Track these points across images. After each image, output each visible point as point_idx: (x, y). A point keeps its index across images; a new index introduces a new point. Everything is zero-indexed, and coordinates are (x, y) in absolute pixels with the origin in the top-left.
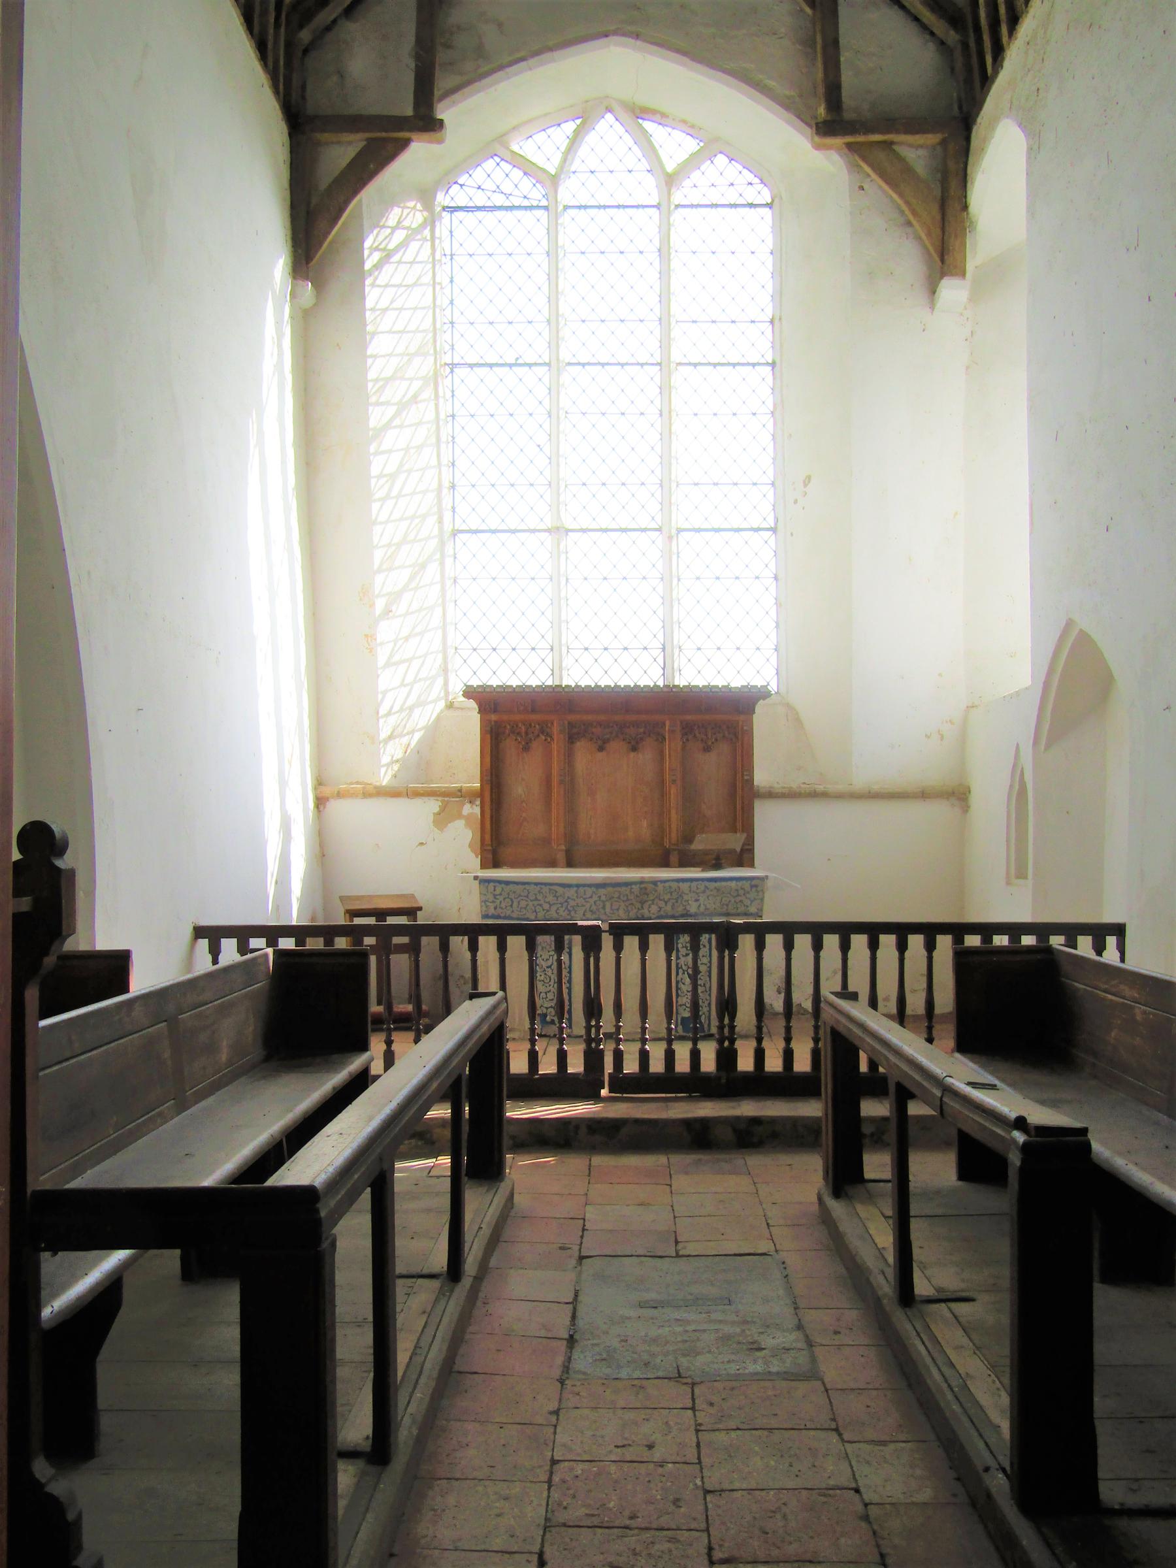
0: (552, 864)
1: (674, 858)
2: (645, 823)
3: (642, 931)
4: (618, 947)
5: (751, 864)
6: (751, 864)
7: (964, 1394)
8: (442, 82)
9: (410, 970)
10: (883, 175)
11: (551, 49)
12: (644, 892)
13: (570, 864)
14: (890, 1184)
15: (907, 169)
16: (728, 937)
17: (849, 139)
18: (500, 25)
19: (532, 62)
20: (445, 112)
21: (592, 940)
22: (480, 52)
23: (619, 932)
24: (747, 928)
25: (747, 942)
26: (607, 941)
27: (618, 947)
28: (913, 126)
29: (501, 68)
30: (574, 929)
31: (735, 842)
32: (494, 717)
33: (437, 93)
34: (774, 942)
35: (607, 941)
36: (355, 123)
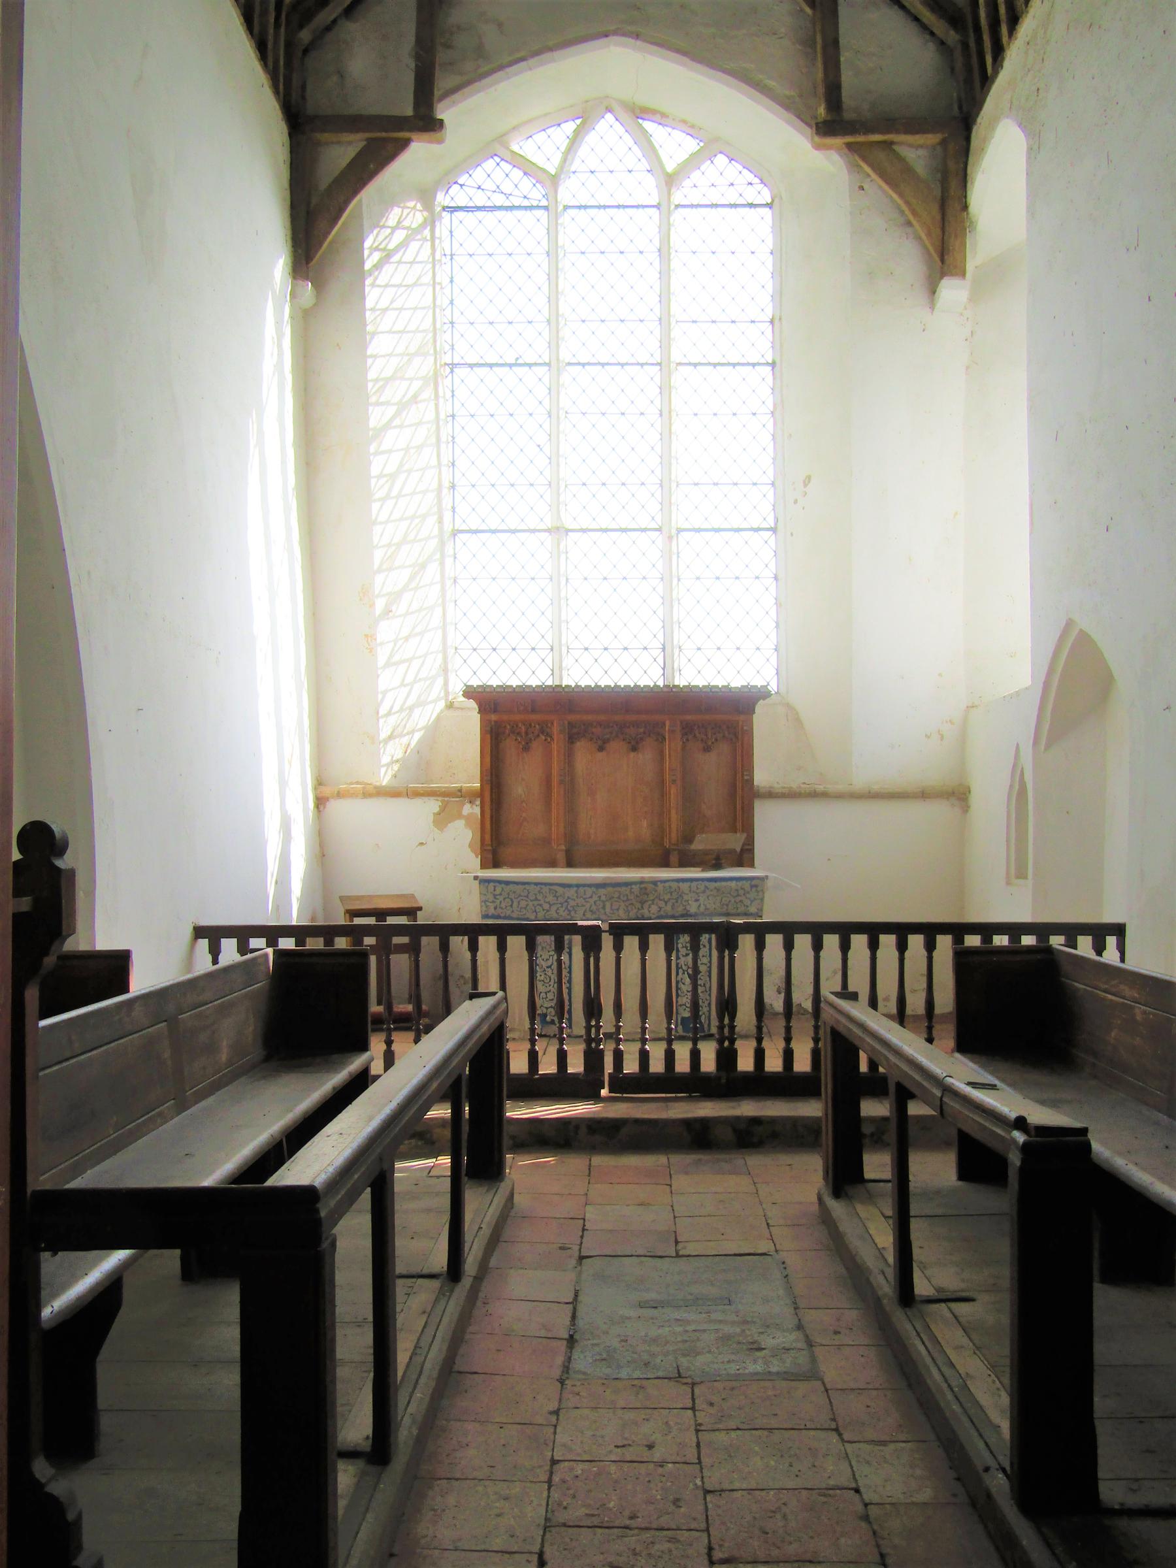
0: (552, 864)
1: (674, 858)
2: (645, 823)
3: (642, 931)
4: (618, 947)
5: (751, 864)
6: (751, 864)
7: (964, 1394)
8: (442, 82)
9: (410, 970)
10: (883, 175)
11: (551, 49)
12: (644, 892)
13: (570, 864)
14: (890, 1184)
15: (907, 169)
16: (728, 937)
17: (849, 139)
18: (500, 25)
19: (532, 62)
20: (445, 112)
21: (592, 940)
22: (480, 52)
23: (619, 932)
24: (747, 928)
25: (747, 942)
26: (607, 941)
27: (618, 947)
28: (913, 126)
29: (501, 68)
30: (574, 929)
31: (735, 842)
32: (494, 717)
33: (437, 93)
34: (774, 942)
35: (607, 941)
36: (355, 123)
